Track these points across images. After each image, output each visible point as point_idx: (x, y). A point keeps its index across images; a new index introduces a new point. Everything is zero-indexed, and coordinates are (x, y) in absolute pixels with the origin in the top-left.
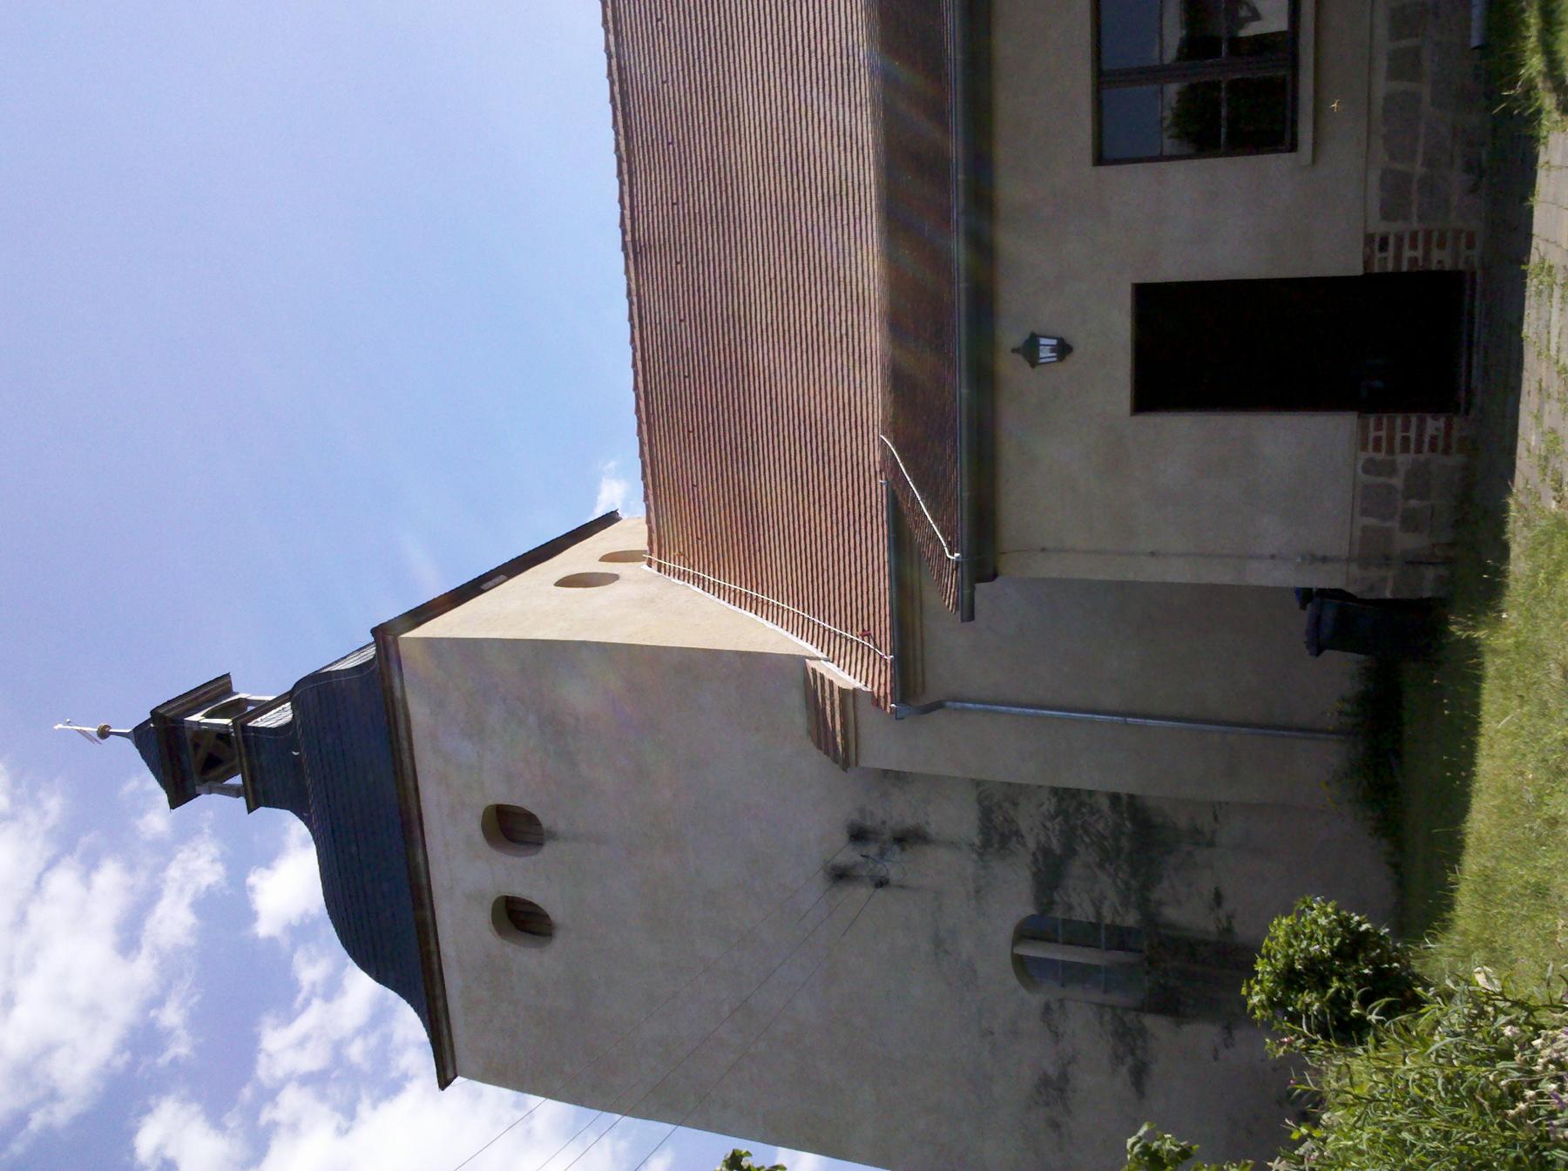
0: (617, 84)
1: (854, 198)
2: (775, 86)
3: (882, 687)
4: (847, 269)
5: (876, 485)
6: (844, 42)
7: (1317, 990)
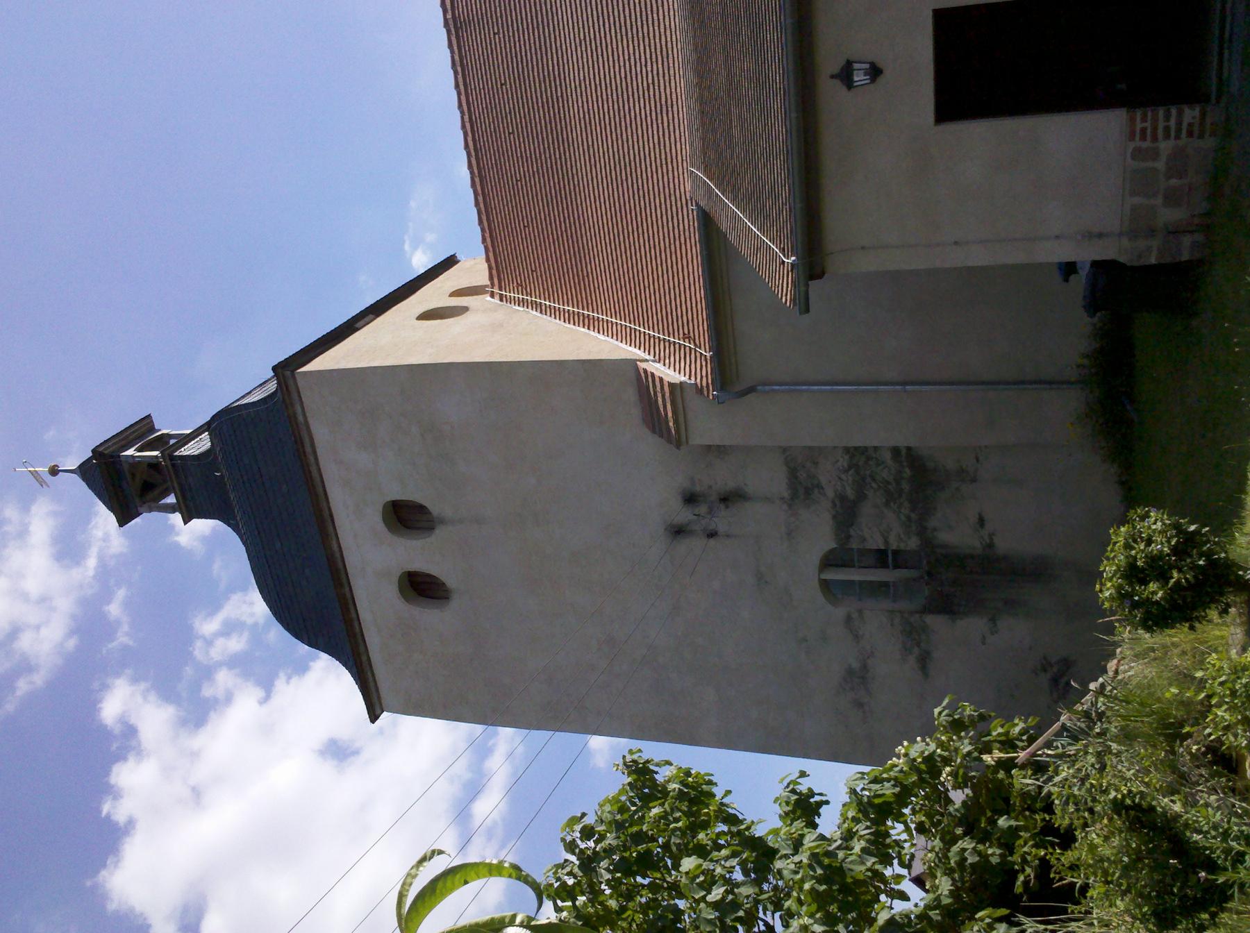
3: (704, 379)
4: (651, 25)
5: (688, 211)
7: (1158, 581)
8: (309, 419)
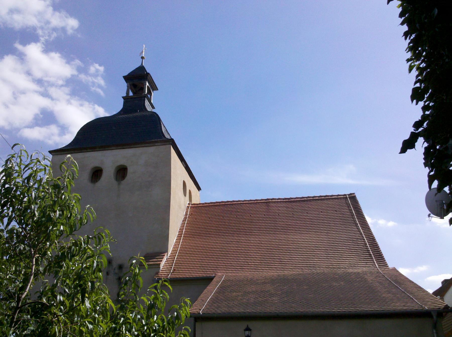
0: (306, 199)
8: (155, 147)
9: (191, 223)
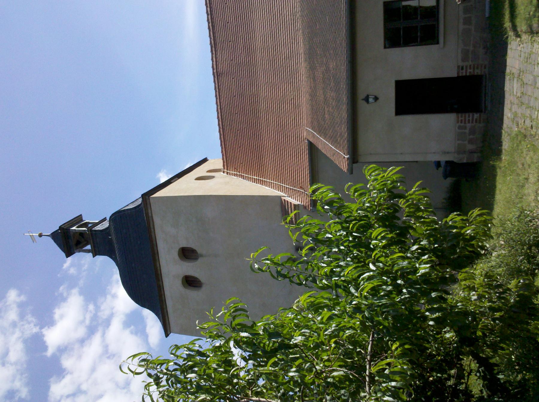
0: (211, 23)
1: (295, 57)
2: (267, 24)
3: (307, 203)
4: (293, 79)
6: (292, 11)
9: (246, 169)
